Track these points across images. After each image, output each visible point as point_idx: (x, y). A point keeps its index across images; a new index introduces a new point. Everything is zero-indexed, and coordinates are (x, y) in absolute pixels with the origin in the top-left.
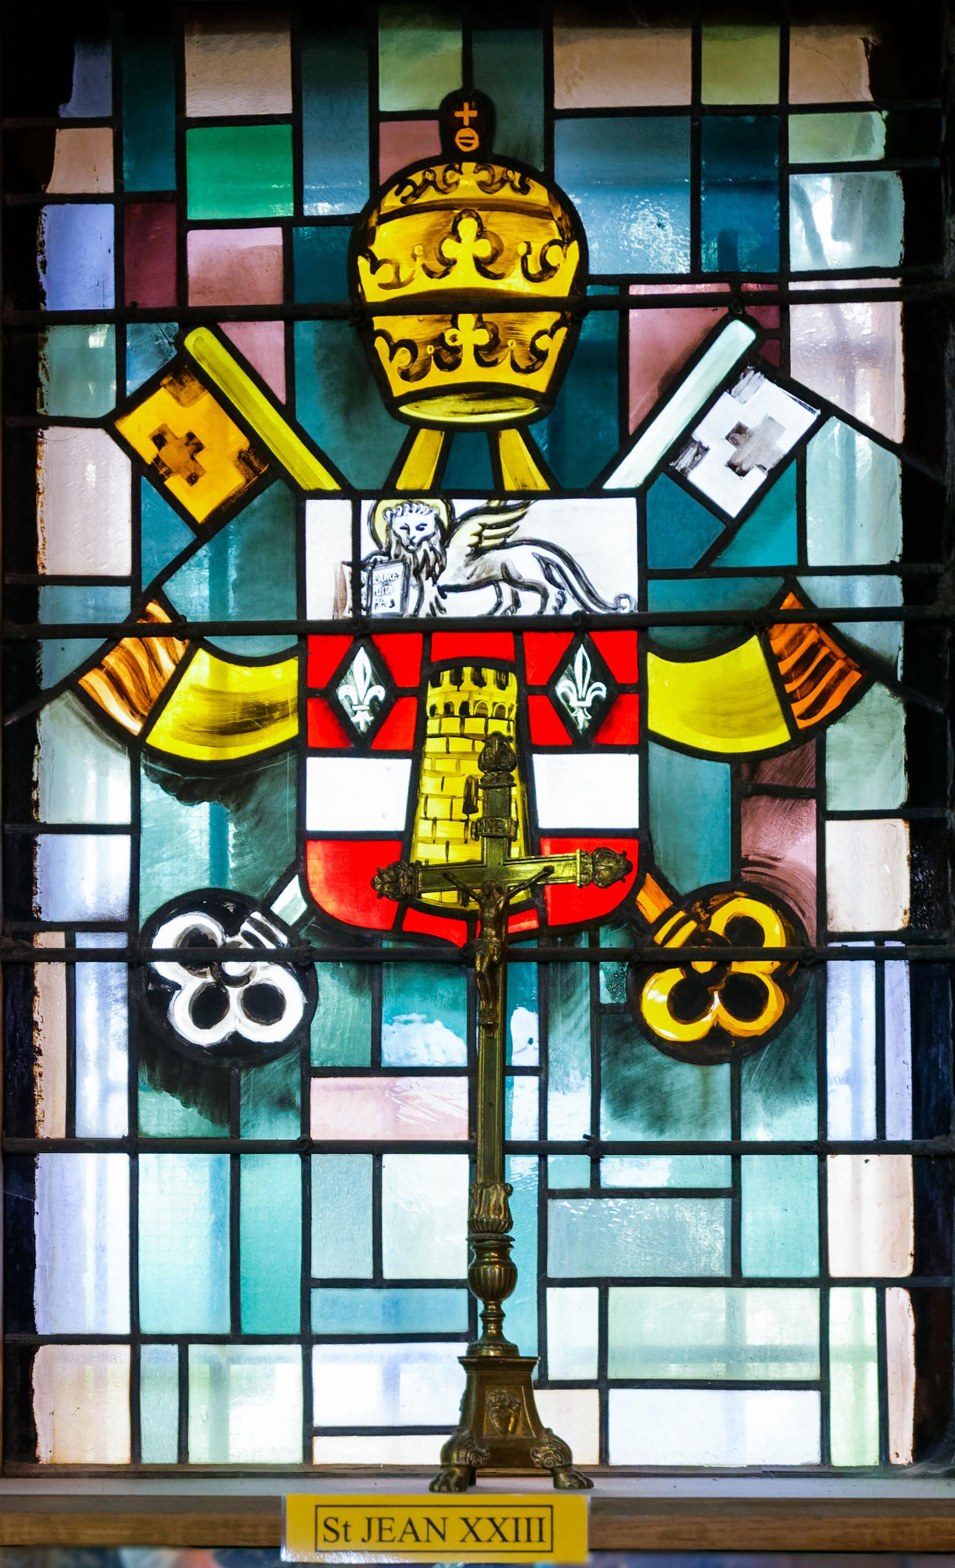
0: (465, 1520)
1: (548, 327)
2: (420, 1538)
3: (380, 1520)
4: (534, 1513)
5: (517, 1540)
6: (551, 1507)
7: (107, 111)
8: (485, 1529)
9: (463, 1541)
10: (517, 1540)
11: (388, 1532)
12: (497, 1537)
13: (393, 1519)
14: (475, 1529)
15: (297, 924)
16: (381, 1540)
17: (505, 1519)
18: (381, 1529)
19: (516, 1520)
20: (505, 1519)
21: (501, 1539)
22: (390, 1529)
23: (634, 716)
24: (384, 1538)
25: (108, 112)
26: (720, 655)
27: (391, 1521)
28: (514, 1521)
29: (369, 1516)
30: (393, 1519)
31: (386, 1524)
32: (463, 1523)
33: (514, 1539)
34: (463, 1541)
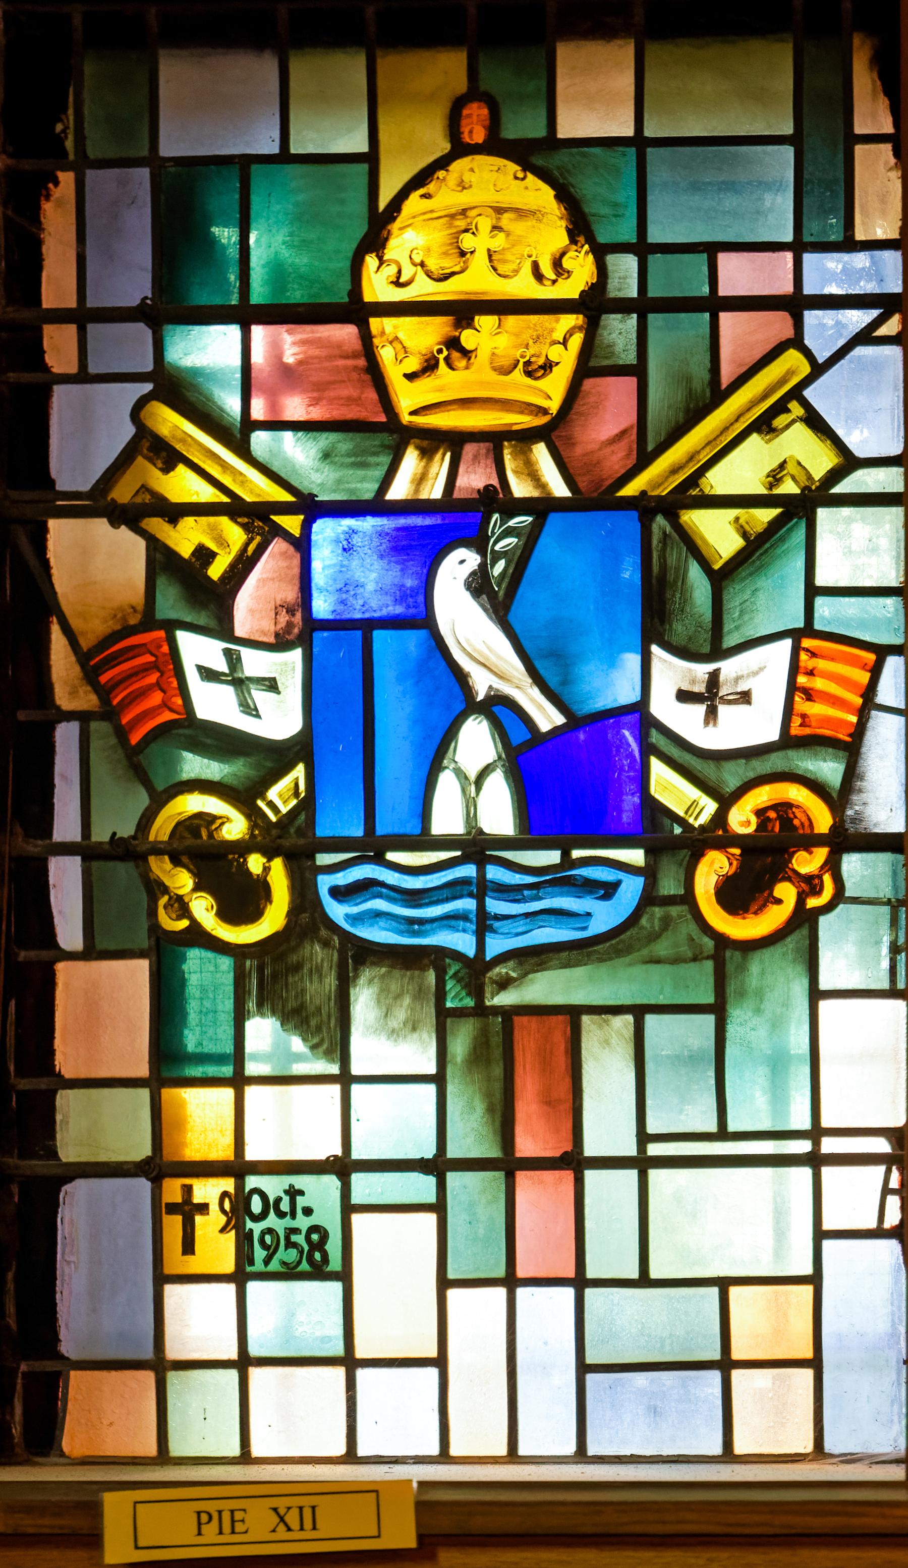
0: (275, 1510)
1: (377, 262)
2: (292, 1527)
3: (232, 1512)
4: (306, 1501)
5: (302, 1529)
6: (377, 1491)
7: (788, 129)
8: (292, 1519)
9: (274, 1531)
10: (302, 1529)
11: (241, 1523)
12: (282, 1527)
13: (244, 1510)
14: (278, 1520)
15: (141, 955)
16: (233, 1532)
17: (289, 1508)
18: (233, 1522)
19: (301, 1508)
20: (289, 1508)
21: (285, 1529)
22: (243, 1521)
23: (799, 563)
24: (237, 1530)
25: (788, 129)
26: (253, 568)
27: (242, 1512)
28: (297, 1510)
29: (300, 1505)
30: (244, 1510)
31: (238, 1516)
32: (273, 1513)
33: (298, 1527)
34: (274, 1531)
